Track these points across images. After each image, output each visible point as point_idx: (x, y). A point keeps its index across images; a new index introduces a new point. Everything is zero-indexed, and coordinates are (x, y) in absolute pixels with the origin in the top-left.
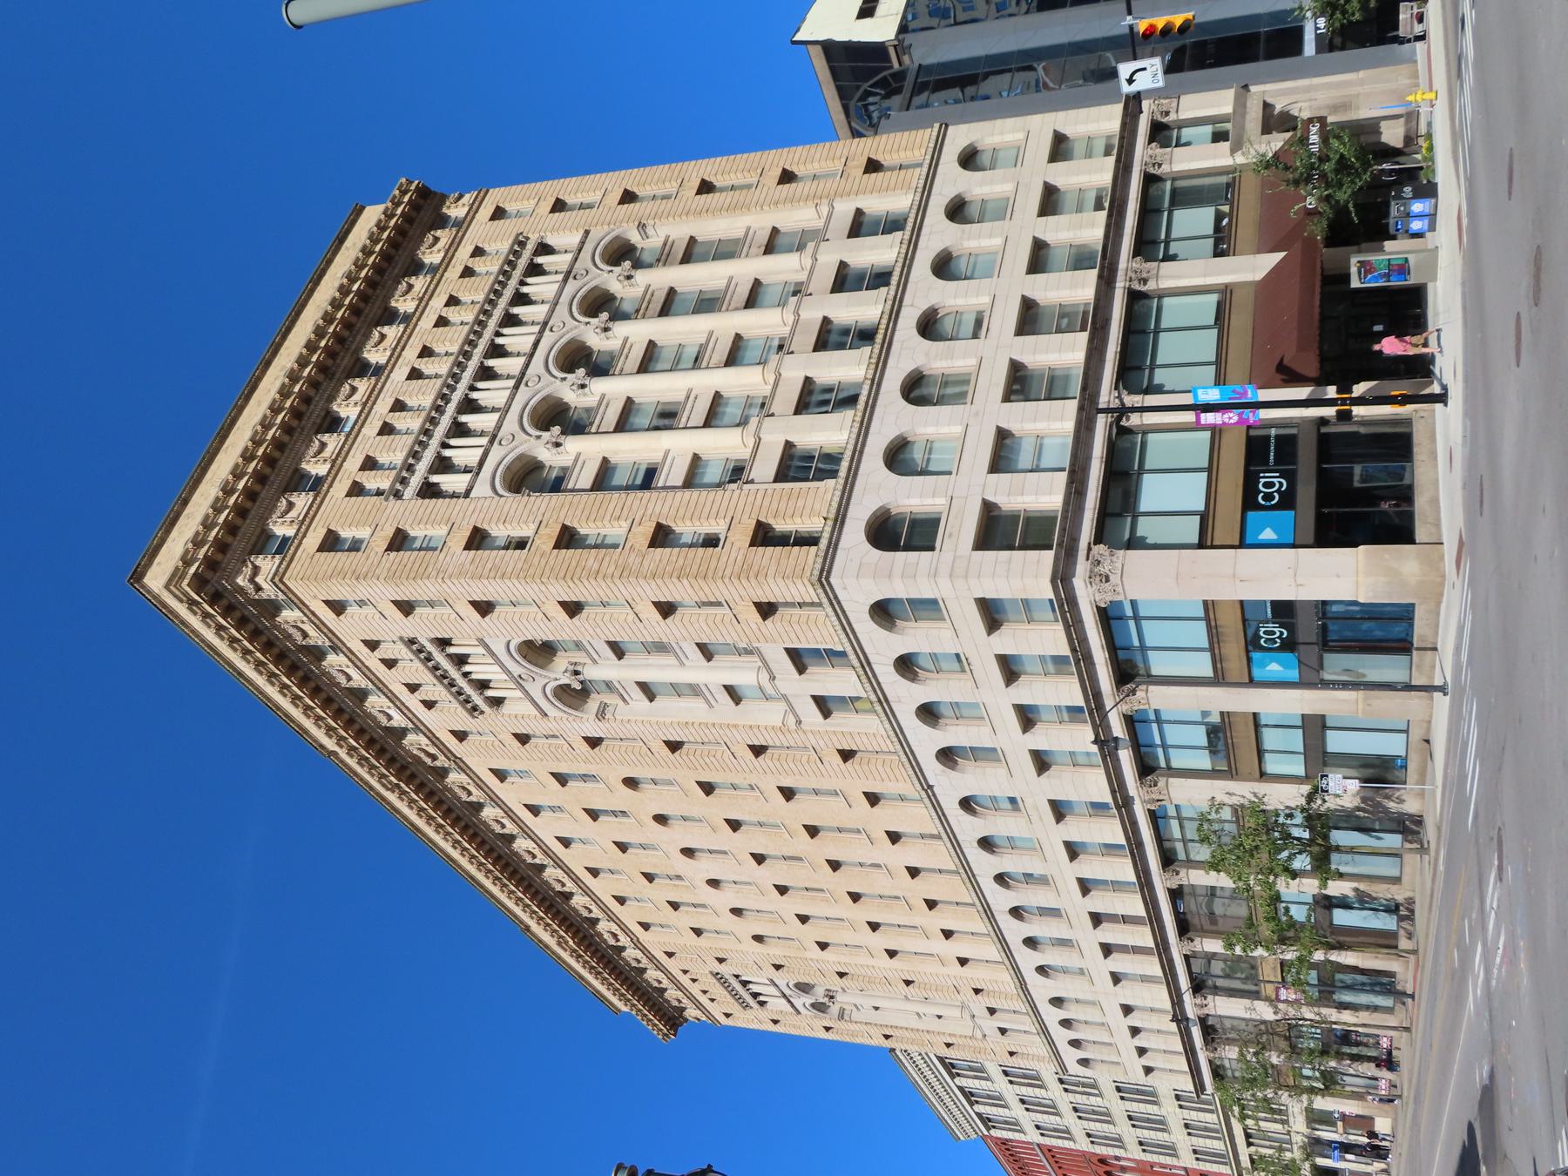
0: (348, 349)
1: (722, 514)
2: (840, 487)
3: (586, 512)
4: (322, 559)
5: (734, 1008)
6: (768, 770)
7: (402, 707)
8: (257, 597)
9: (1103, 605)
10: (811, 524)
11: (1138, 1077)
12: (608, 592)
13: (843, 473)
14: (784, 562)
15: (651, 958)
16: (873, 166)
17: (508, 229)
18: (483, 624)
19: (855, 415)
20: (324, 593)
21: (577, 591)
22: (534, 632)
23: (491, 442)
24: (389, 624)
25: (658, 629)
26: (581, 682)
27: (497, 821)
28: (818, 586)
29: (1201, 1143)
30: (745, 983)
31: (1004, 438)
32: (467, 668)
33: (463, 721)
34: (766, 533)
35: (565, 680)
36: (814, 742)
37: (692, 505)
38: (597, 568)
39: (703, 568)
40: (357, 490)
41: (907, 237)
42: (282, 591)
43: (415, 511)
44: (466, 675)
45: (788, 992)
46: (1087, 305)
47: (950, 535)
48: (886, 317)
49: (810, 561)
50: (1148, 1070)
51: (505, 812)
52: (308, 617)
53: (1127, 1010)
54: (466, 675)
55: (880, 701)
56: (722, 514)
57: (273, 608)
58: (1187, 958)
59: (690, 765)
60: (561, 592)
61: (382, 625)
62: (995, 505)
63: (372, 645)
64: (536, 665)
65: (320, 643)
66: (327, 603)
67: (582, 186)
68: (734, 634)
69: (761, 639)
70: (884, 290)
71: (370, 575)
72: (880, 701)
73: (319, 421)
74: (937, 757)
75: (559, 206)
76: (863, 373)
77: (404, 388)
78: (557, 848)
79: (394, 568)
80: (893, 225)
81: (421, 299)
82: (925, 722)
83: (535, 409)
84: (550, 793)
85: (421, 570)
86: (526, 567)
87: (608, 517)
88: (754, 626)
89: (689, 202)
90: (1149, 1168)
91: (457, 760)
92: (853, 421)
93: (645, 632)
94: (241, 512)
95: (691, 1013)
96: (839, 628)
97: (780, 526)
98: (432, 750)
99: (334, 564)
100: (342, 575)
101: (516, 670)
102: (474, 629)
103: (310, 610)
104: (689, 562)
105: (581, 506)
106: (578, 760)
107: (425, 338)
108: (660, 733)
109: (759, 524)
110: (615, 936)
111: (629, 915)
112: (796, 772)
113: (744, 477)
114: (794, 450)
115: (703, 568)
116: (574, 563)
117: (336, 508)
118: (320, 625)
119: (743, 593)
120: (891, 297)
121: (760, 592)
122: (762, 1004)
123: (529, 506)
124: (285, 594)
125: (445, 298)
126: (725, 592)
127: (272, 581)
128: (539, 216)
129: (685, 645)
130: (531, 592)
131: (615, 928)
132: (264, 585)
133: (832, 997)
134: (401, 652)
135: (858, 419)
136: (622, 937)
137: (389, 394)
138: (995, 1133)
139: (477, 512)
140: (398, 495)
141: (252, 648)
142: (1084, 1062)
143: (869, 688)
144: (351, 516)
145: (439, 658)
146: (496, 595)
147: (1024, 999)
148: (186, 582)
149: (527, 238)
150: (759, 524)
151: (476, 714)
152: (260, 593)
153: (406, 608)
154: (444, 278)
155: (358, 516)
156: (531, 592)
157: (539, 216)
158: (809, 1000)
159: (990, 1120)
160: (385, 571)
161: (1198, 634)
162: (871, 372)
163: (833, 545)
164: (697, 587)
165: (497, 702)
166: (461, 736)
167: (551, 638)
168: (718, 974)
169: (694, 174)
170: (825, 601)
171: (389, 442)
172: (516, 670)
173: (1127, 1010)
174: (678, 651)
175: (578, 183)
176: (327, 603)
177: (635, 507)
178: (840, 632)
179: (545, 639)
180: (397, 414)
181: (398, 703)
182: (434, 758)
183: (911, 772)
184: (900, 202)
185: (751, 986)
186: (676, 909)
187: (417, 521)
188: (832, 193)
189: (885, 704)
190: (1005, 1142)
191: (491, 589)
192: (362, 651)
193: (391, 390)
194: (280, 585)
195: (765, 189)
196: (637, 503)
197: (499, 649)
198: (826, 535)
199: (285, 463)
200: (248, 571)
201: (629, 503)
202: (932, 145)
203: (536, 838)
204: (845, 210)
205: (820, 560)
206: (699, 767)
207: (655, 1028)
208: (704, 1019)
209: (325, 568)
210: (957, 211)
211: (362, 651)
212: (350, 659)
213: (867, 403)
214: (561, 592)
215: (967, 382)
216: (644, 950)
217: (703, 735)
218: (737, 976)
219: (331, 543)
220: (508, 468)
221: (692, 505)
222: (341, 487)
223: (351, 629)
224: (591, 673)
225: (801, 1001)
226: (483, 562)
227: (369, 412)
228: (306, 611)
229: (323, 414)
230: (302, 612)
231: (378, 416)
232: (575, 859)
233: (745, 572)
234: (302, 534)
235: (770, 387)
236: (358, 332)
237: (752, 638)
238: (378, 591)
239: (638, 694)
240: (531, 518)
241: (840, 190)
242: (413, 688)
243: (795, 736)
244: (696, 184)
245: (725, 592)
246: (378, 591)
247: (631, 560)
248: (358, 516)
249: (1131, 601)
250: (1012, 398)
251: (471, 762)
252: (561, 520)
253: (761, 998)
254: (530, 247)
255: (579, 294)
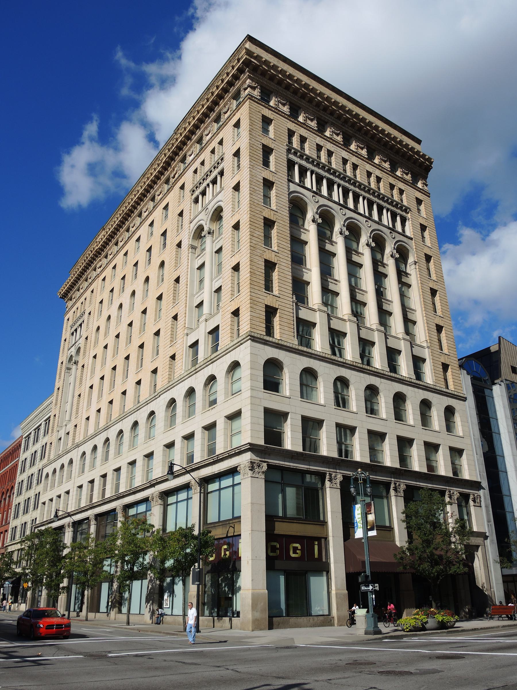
0: (356, 132)
1: (281, 292)
2: (294, 346)
3: (281, 232)
4: (259, 116)
5: (70, 322)
6: (167, 323)
7: (194, 160)
8: (241, 89)
9: (238, 469)
10: (277, 334)
11: (41, 501)
12: (244, 241)
13: (301, 348)
14: (258, 320)
15: (91, 284)
16: (445, 367)
17: (413, 205)
18: (230, 189)
19: (329, 354)
20: (243, 118)
21: (244, 227)
22: (226, 211)
23: (314, 192)
24: (230, 147)
25: (227, 266)
26: (205, 236)
27: (147, 210)
28: (247, 335)
29: (19, 529)
30: (81, 325)
31: (318, 423)
32: (211, 185)
33: (189, 187)
34: (272, 313)
35: (206, 229)
36: (178, 342)
37: (285, 279)
38: (254, 236)
39: (255, 283)
40: (291, 134)
41: (413, 381)
42: (244, 99)
43: (281, 157)
44: (208, 185)
45: (77, 344)
46: (383, 463)
47: (270, 396)
48: (375, 370)
49: (258, 332)
50: (44, 503)
51: (150, 212)
52: (233, 112)
53: (68, 493)
54: (208, 185)
55: (196, 369)
56: (281, 292)
57: (236, 96)
58: (88, 518)
59: (169, 289)
60: (244, 220)
61: (229, 146)
62: (286, 420)
63: (221, 143)
64: (212, 215)
65: (222, 120)
66: (239, 120)
67: (433, 238)
68: (225, 300)
69: (223, 313)
70: (388, 370)
71: (251, 136)
72: (196, 369)
73: (322, 118)
74: (172, 398)
75: (423, 228)
76: (349, 359)
77: (338, 156)
78: (136, 237)
79: (255, 147)
80: (418, 374)
81: (380, 166)
82: (187, 391)
83: (330, 212)
84: (158, 230)
85: (253, 158)
86: (255, 204)
87: (279, 242)
88: (229, 308)
89: (426, 284)
90: (9, 508)
91: (172, 188)
92: (326, 354)
93: (226, 260)
94: (280, 82)
95: (70, 304)
96: (228, 347)
97: (276, 321)
98: (176, 176)
99: (256, 121)
100: (251, 124)
101: (210, 207)
102: (228, 185)
103: (236, 113)
104: (258, 277)
105: (283, 230)
106: (172, 240)
107: (362, 166)
108: (183, 273)
109: (276, 310)
110: (100, 267)
111: (108, 272)
112: (166, 336)
113: (299, 304)
114: (312, 328)
115: (255, 283)
116: (257, 225)
117: (283, 124)
118: (229, 118)
119: (243, 302)
120: (385, 372)
121: (244, 309)
122: (73, 334)
123: (284, 207)
124: (243, 101)
125: (380, 176)
126: (244, 294)
127: (249, 94)
128: (418, 218)
129: (221, 280)
130: (244, 207)
131: (103, 266)
132: (247, 91)
133: (75, 363)
134: (216, 157)
135: (327, 356)
136: (99, 270)
137: (336, 149)
138: (24, 440)
139: (281, 184)
140: (289, 151)
141: (241, 62)
142: (47, 475)
143: (201, 364)
144: (279, 130)
145: (215, 172)
146: (242, 192)
147: (72, 447)
148: (248, 57)
149: (408, 213)
150: (276, 310)
151: (191, 192)
152: (243, 91)
153: (237, 154)
154: (389, 176)
155: (279, 133)
156: (244, 207)
157: (418, 218)
158: (73, 354)
159: (29, 438)
160: (253, 143)
161: (226, 515)
162: (349, 363)
163: (265, 343)
164: (246, 280)
165: (196, 201)
166: (182, 187)
167: (224, 219)
168: (84, 313)
169: (440, 287)
170: (240, 339)
171: (313, 148)
172: (210, 207)
173: (68, 493)
174: (219, 277)
175: (434, 236)
176: (239, 120)
177: (283, 254)
178: (226, 348)
179: (223, 217)
180: (326, 152)
181: (196, 158)
182: (174, 177)
183: (165, 387)
184: (429, 378)
185: (80, 328)
186: (110, 291)
187: (277, 158)
188: (433, 348)
189: (194, 372)
190: (20, 445)
191: (245, 189)
192: (218, 139)
193: (338, 150)
194: (246, 98)
195: (433, 318)
196: (286, 255)
197: (219, 198)
198: (271, 339)
199: (303, 103)
200: (253, 84)
201: (286, 251)
202: (456, 393)
203: (140, 226)
204: (426, 354)
205: (259, 336)
206: (168, 293)
207: (63, 290)
208: (67, 310)
209: (255, 117)
210: (426, 405)
211: (218, 139)
212: (215, 134)
213: (334, 360)
214: (244, 220)
215: (344, 406)
216: (94, 280)
217: (182, 293)
218: (83, 322)
219: (266, 121)
220: (302, 199)
221: (285, 279)
222: (292, 126)
223: (227, 133)
224: (208, 240)
225: (73, 351)
226: (258, 186)
227: (327, 140)
228: (236, 111)
229: (326, 121)
230: (235, 110)
231: (326, 144)
232: (131, 245)
233: (253, 302)
234: (270, 108)
235: (341, 317)
236: (364, 137)
237: (223, 309)
238: (244, 140)
239: (200, 263)
240: (278, 208)
241: (435, 352)
242: (203, 163)
243: (181, 334)
244: (435, 288)
245: (244, 294)
246: (244, 140)
247: (258, 251)
248: (279, 133)
249: (240, 483)
250: (338, 428)
251: (172, 194)
252: (277, 221)
253: (75, 333)
254: (404, 214)
255: (383, 234)
